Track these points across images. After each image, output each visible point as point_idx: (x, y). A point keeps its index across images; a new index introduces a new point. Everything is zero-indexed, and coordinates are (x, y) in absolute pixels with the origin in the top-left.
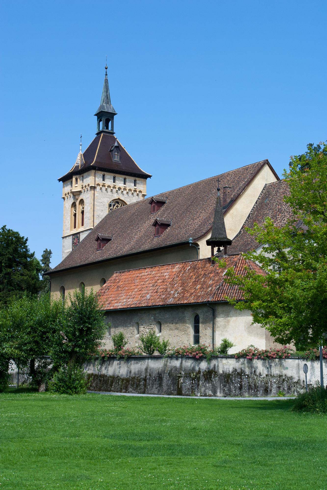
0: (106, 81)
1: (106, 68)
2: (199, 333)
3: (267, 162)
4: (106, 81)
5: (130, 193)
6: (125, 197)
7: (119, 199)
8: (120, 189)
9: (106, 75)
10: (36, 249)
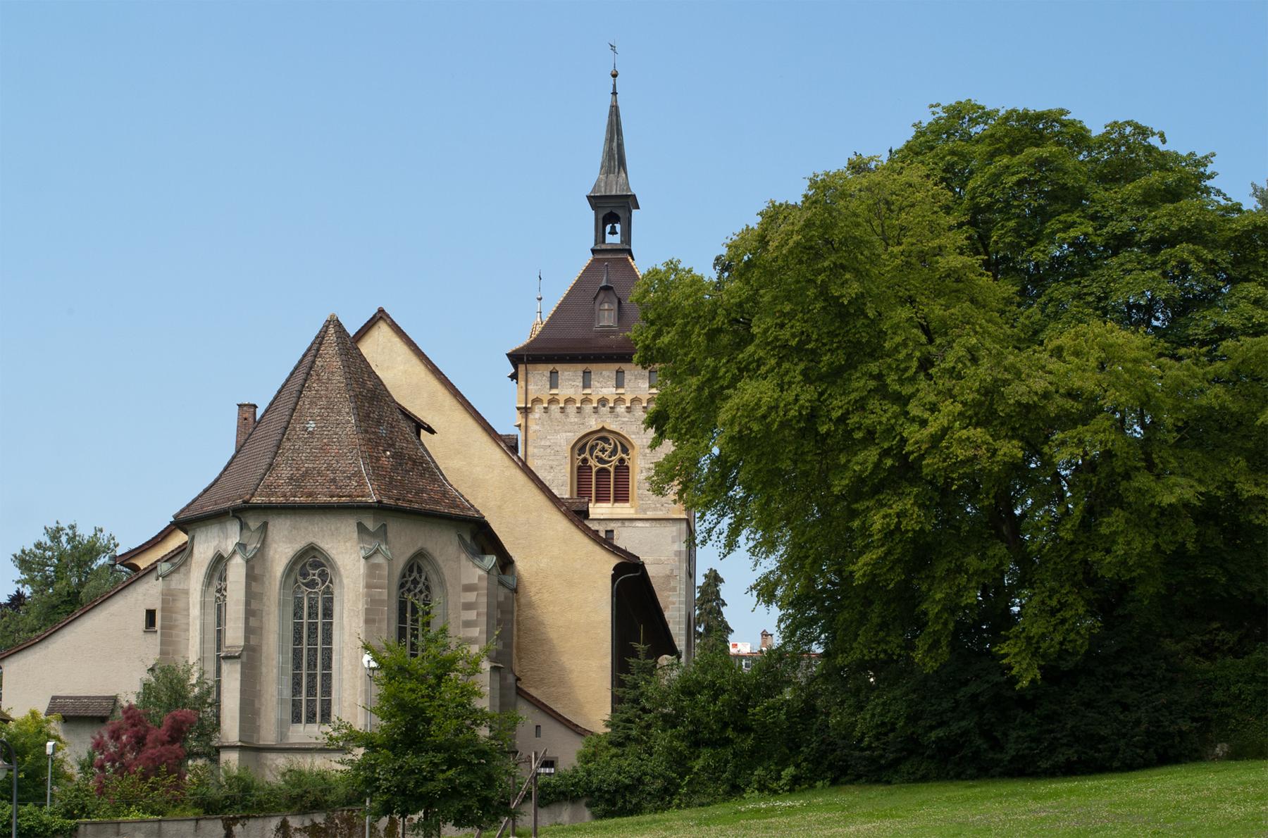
0: (615, 112)
1: (615, 76)
2: (330, 643)
3: (381, 316)
4: (615, 112)
5: (571, 409)
6: (624, 423)
7: (603, 429)
8: (603, 401)
9: (615, 93)
10: (732, 639)
